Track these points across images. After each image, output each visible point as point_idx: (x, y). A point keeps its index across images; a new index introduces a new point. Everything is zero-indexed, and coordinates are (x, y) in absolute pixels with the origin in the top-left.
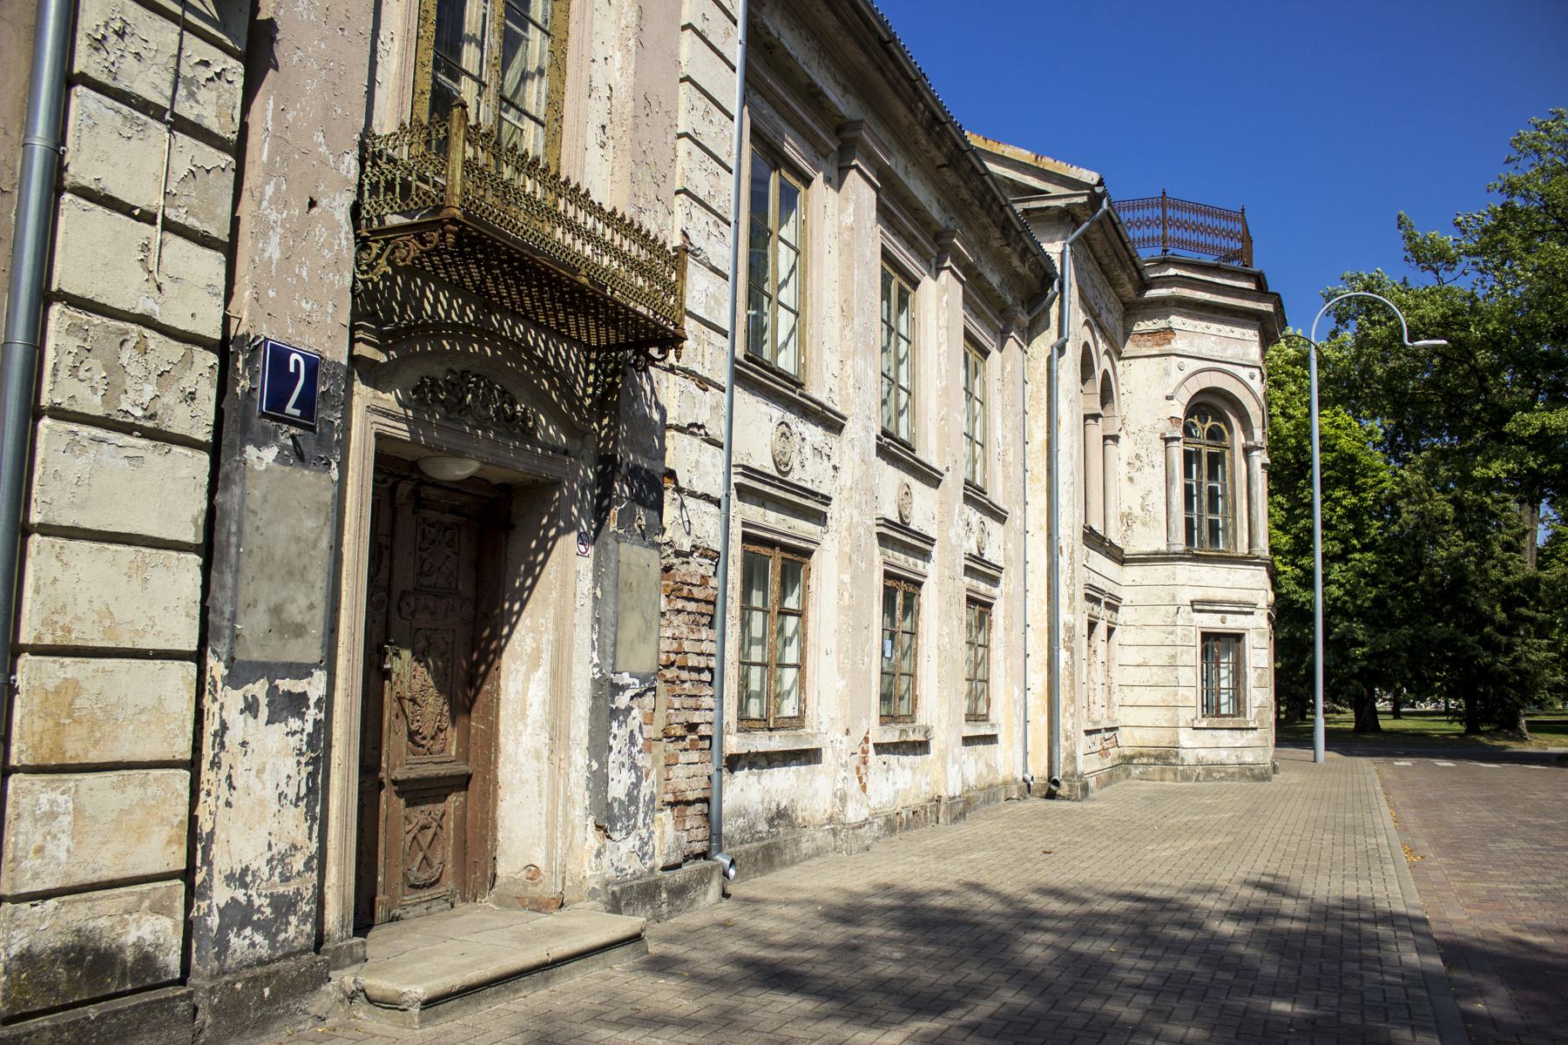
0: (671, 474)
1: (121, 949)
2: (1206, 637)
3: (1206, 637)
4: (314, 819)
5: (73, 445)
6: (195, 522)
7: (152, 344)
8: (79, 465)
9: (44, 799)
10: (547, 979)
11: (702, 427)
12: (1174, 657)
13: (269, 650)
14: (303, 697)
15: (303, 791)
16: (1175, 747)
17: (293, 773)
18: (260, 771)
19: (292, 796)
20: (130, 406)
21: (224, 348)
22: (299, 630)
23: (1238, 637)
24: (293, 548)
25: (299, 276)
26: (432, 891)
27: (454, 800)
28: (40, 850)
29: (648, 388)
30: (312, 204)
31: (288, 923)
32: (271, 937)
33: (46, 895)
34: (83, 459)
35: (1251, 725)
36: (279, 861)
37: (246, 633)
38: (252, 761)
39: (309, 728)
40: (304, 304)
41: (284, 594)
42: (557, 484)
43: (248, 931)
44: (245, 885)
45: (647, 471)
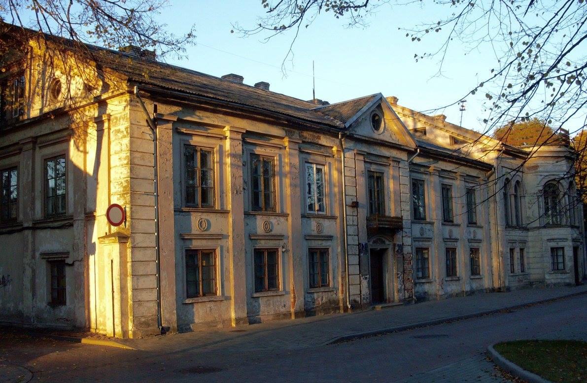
2: (553, 249)
3: (553, 249)
12: (543, 255)
16: (544, 278)
21: (358, 245)
22: (366, 271)
23: (563, 248)
35: (568, 272)
36: (138, 25)
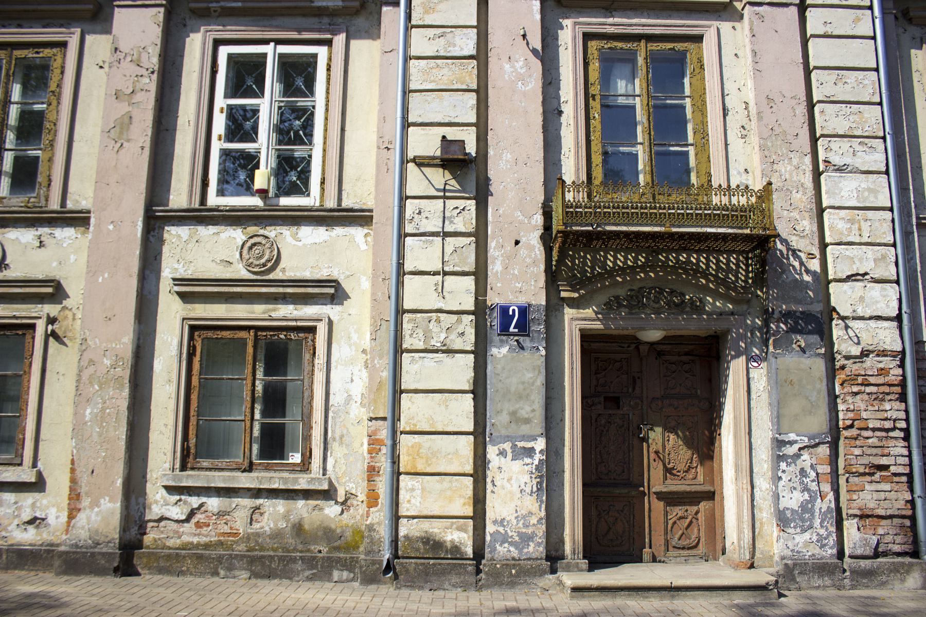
0: (834, 309)
1: (445, 542)
4: (541, 502)
5: (413, 360)
6: (469, 382)
7: (442, 319)
8: (416, 367)
9: (409, 484)
10: (673, 597)
11: (866, 274)
13: (510, 430)
14: (532, 450)
15: (535, 489)
17: (528, 481)
18: (509, 480)
19: (528, 490)
20: (436, 343)
24: (521, 387)
25: (514, 274)
26: (689, 552)
27: (703, 505)
28: (409, 501)
29: (796, 264)
30: (517, 243)
31: (528, 545)
32: (521, 551)
33: (414, 517)
34: (417, 366)
37: (497, 423)
38: (506, 475)
39: (536, 462)
40: (517, 285)
41: (517, 406)
42: (728, 331)
43: (506, 545)
44: (504, 526)
45: (802, 313)
